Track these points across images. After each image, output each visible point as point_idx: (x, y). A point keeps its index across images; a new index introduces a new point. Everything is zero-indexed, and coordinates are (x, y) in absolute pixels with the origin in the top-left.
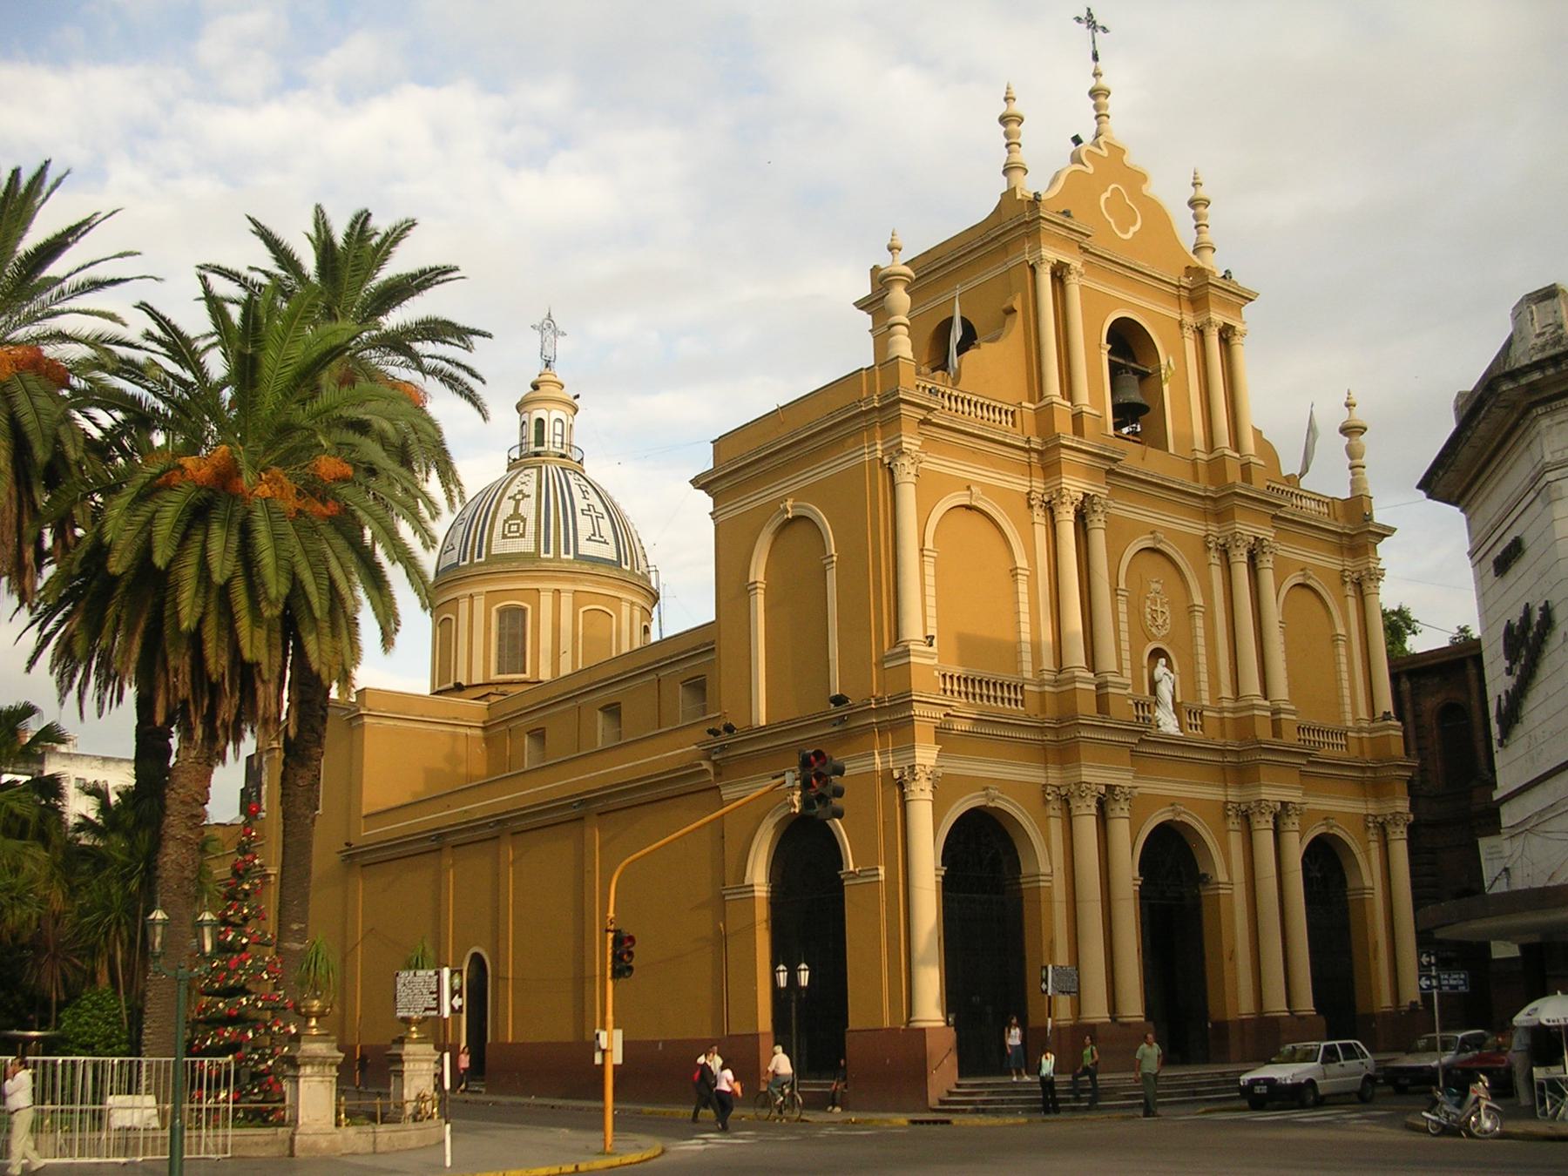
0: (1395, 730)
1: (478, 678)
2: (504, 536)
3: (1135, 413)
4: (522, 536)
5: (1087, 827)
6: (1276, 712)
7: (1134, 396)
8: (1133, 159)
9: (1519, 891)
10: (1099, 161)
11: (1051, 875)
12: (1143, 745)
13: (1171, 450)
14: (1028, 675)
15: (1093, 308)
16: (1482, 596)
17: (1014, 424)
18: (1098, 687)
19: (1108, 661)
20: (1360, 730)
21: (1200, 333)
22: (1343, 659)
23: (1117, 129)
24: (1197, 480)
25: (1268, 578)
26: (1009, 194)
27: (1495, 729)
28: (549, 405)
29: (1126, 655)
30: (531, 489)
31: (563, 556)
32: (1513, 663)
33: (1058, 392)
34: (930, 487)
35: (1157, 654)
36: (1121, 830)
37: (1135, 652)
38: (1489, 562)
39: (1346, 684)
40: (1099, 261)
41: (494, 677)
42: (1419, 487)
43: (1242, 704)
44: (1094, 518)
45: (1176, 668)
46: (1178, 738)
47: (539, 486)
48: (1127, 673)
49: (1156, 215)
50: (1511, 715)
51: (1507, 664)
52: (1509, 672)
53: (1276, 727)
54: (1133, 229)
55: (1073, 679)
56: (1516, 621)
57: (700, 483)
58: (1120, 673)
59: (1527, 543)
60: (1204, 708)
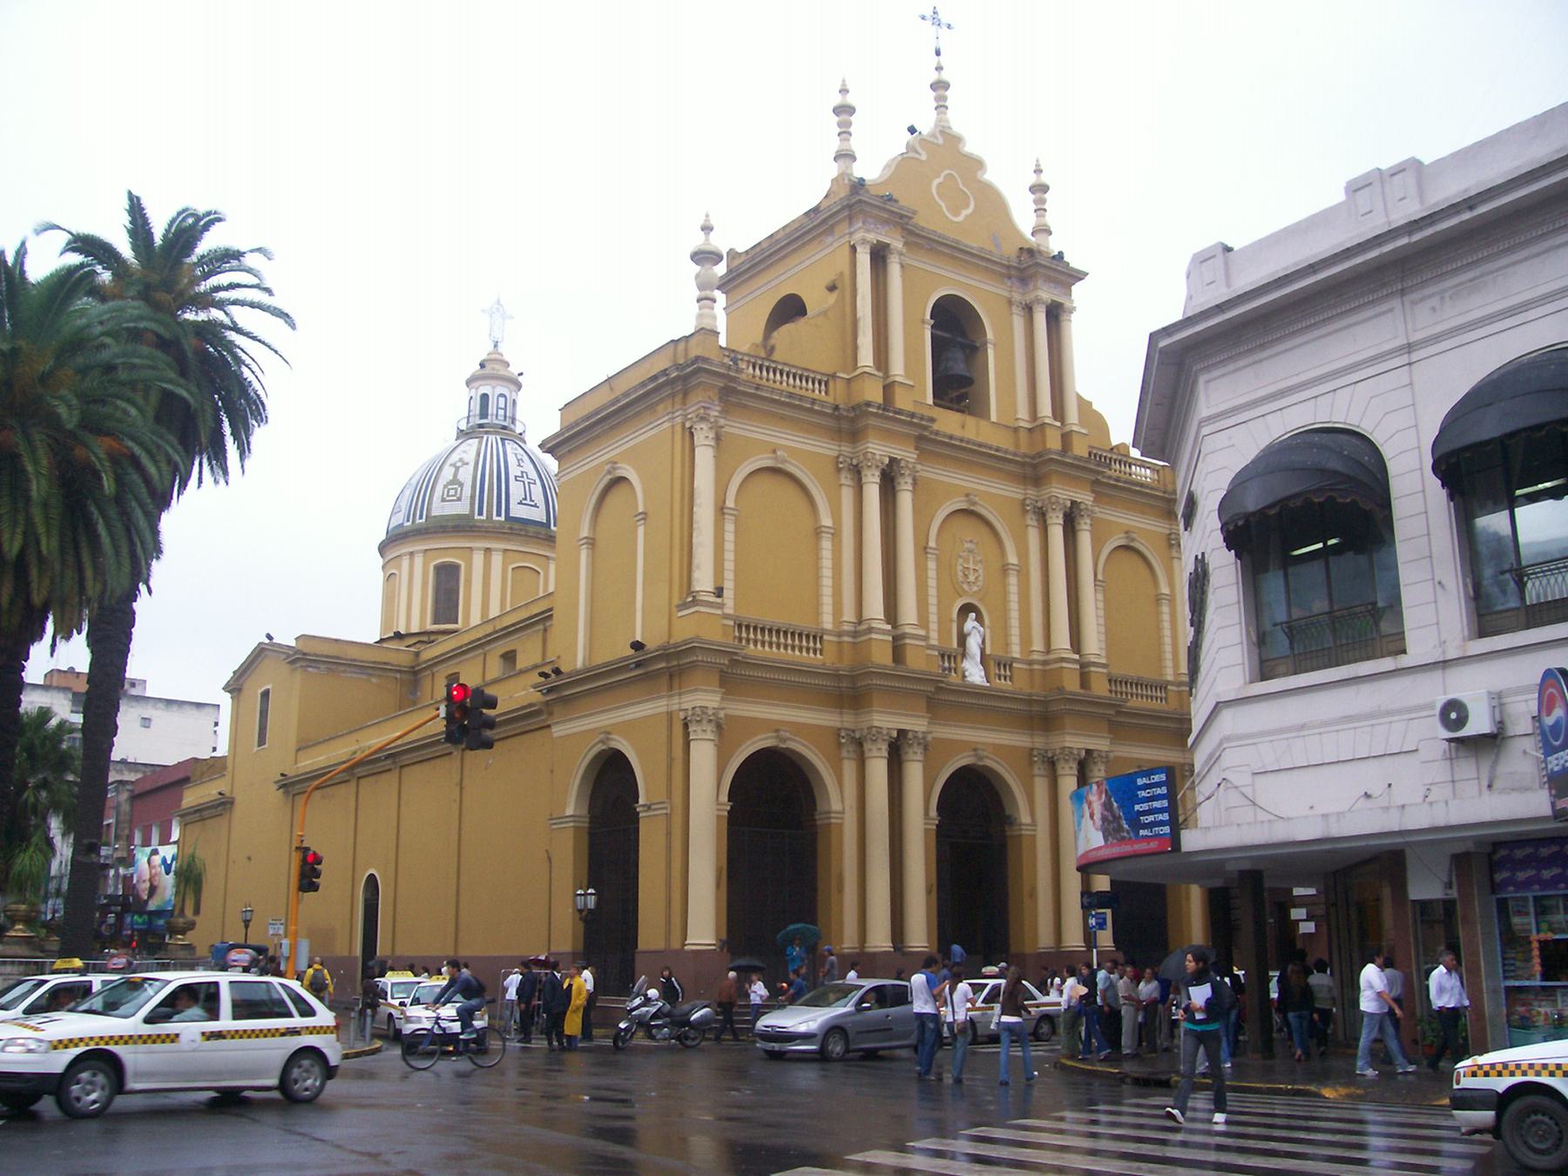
1: (415, 629)
2: (443, 500)
3: (957, 384)
5: (878, 769)
8: (971, 147)
9: (116, 709)
10: (940, 154)
11: (843, 812)
12: (943, 696)
13: (994, 418)
19: (908, 613)
22: (1167, 625)
23: (957, 121)
28: (494, 382)
31: (495, 518)
35: (966, 609)
36: (914, 773)
39: (1168, 640)
41: (430, 627)
43: (1052, 656)
45: (987, 622)
49: (992, 201)
53: (1085, 681)
54: (965, 213)
55: (870, 630)
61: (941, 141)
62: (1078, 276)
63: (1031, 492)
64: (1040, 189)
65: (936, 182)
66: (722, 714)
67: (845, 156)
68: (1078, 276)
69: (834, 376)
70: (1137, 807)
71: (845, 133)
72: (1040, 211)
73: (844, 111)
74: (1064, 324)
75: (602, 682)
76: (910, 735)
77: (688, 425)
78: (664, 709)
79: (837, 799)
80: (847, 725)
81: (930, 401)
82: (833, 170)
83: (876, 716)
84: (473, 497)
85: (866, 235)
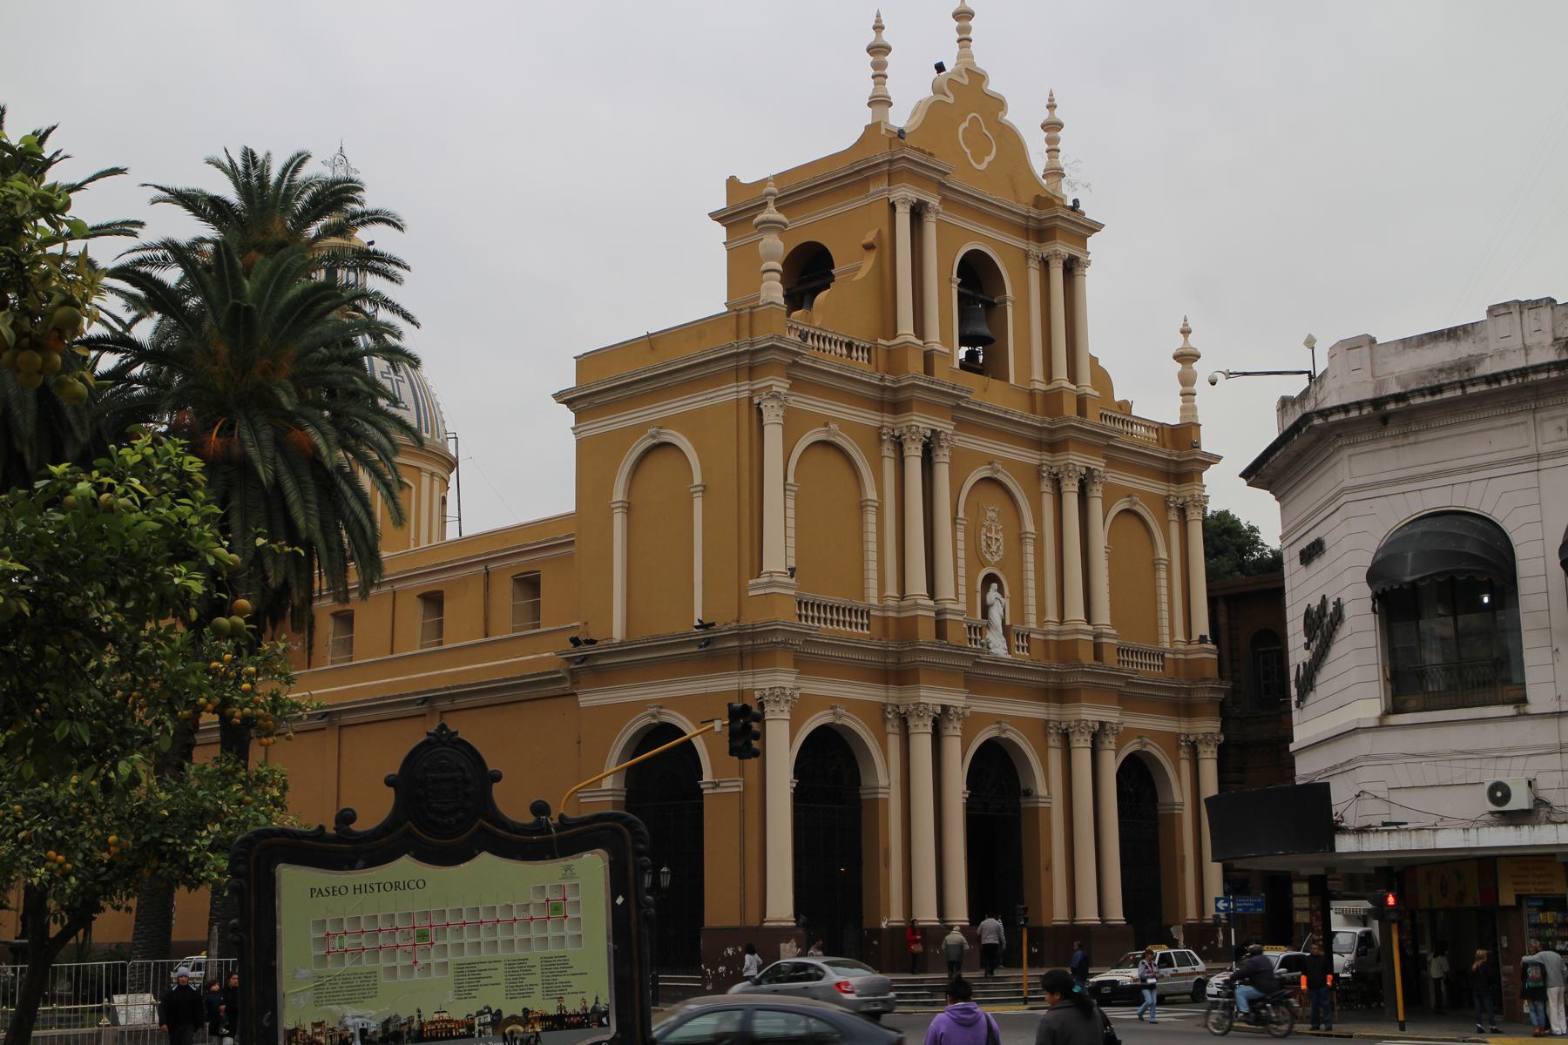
0: (1209, 652)
6: (1097, 636)
8: (994, 86)
10: (966, 96)
12: (981, 675)
13: (1012, 381)
14: (874, 601)
18: (938, 613)
19: (946, 589)
20: (1176, 652)
21: (1045, 264)
24: (1033, 411)
25: (1096, 506)
26: (872, 130)
27: (1294, 691)
29: (962, 581)
32: (1310, 640)
34: (793, 423)
35: (990, 579)
37: (970, 579)
40: (956, 200)
42: (1242, 475)
44: (940, 453)
46: (1009, 661)
48: (963, 598)
49: (1011, 141)
50: (1307, 684)
52: (1307, 647)
54: (988, 159)
55: (916, 606)
58: (957, 600)
59: (1327, 545)
60: (1031, 631)
61: (966, 81)
62: (1094, 228)
63: (888, 419)
64: (1052, 127)
66: (968, 713)
67: (880, 102)
68: (1094, 228)
71: (879, 76)
72: (1053, 151)
73: (878, 50)
74: (1078, 280)
75: (646, 657)
76: (951, 711)
77: (756, 401)
78: (735, 687)
79: (884, 776)
80: (892, 701)
82: (866, 117)
83: (923, 693)
85: (905, 194)
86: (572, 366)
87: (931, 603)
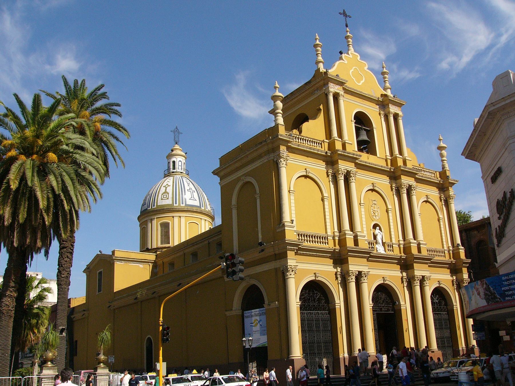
1: (155, 246)
2: (162, 199)
4: (168, 199)
7: (364, 137)
13: (378, 155)
15: (349, 108)
16: (488, 192)
17: (322, 147)
21: (386, 117)
27: (495, 241)
28: (176, 157)
29: (364, 226)
30: (171, 183)
31: (181, 205)
33: (336, 136)
35: (375, 226)
38: (489, 179)
41: (160, 245)
47: (173, 182)
51: (498, 216)
52: (499, 218)
54: (362, 82)
56: (501, 199)
57: (215, 173)
65: (351, 71)
69: (323, 141)
70: (503, 289)
77: (275, 160)
78: (273, 267)
81: (356, 150)
84: (173, 198)
86: (218, 162)
87: (352, 233)
